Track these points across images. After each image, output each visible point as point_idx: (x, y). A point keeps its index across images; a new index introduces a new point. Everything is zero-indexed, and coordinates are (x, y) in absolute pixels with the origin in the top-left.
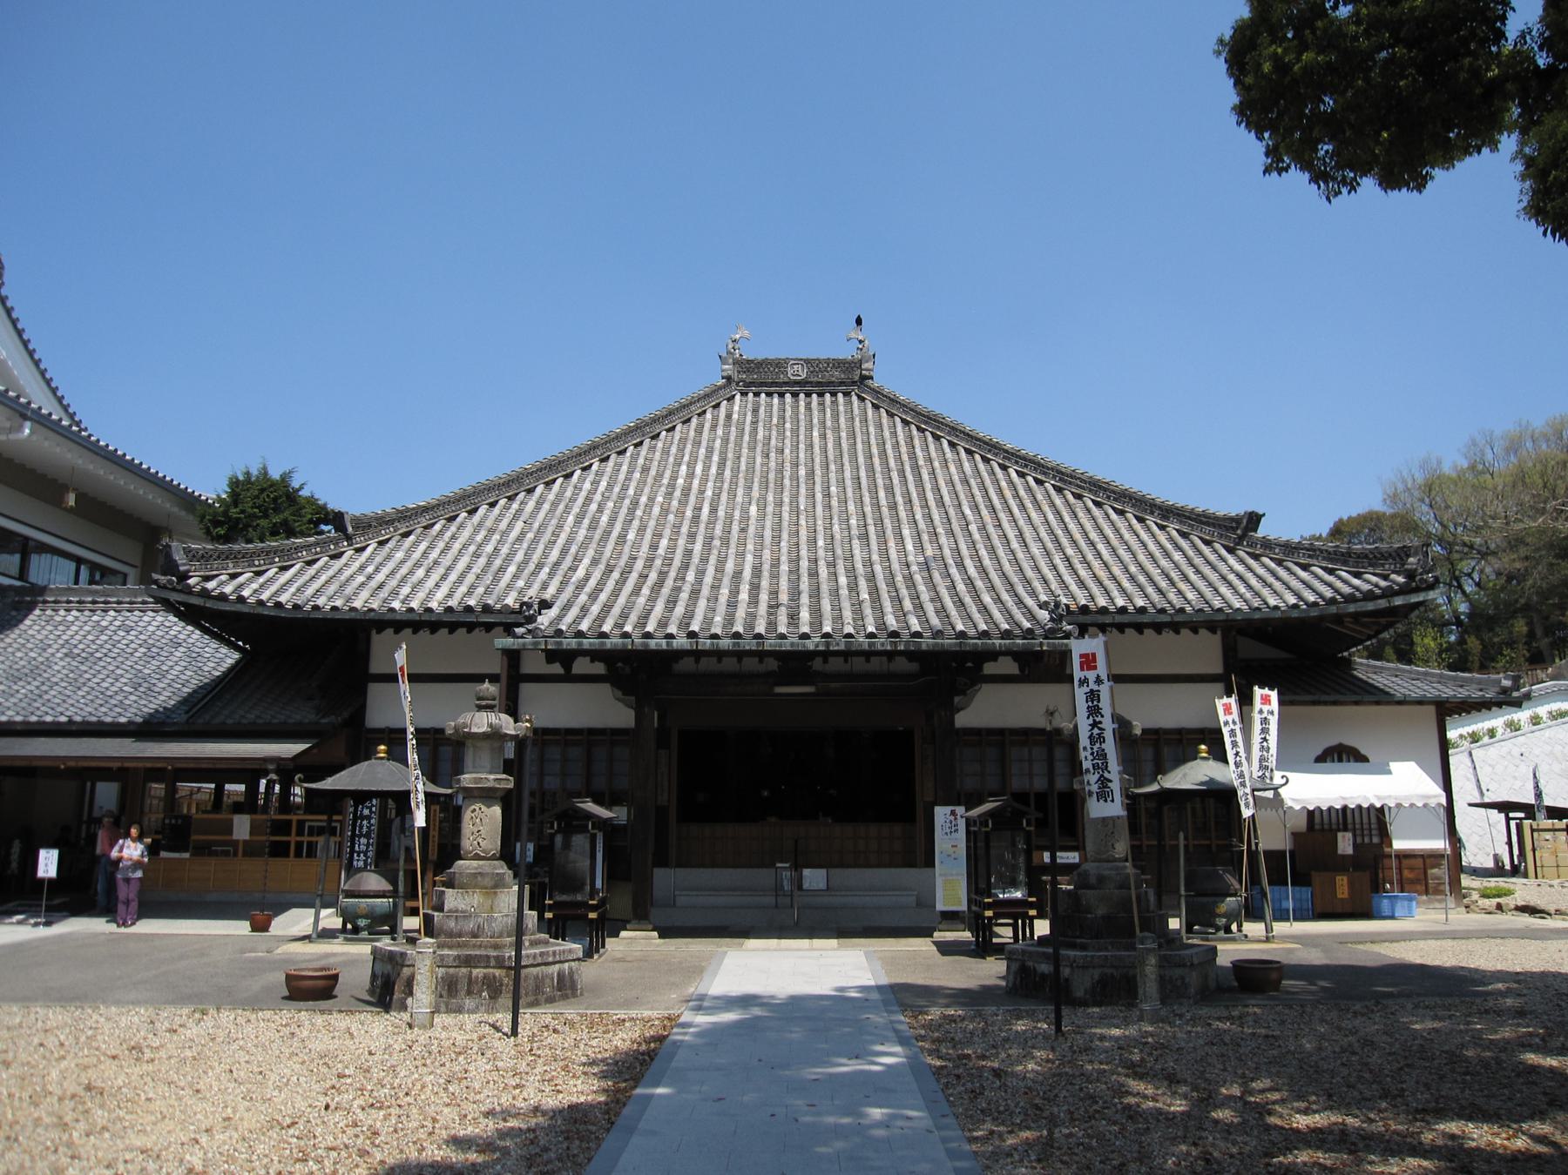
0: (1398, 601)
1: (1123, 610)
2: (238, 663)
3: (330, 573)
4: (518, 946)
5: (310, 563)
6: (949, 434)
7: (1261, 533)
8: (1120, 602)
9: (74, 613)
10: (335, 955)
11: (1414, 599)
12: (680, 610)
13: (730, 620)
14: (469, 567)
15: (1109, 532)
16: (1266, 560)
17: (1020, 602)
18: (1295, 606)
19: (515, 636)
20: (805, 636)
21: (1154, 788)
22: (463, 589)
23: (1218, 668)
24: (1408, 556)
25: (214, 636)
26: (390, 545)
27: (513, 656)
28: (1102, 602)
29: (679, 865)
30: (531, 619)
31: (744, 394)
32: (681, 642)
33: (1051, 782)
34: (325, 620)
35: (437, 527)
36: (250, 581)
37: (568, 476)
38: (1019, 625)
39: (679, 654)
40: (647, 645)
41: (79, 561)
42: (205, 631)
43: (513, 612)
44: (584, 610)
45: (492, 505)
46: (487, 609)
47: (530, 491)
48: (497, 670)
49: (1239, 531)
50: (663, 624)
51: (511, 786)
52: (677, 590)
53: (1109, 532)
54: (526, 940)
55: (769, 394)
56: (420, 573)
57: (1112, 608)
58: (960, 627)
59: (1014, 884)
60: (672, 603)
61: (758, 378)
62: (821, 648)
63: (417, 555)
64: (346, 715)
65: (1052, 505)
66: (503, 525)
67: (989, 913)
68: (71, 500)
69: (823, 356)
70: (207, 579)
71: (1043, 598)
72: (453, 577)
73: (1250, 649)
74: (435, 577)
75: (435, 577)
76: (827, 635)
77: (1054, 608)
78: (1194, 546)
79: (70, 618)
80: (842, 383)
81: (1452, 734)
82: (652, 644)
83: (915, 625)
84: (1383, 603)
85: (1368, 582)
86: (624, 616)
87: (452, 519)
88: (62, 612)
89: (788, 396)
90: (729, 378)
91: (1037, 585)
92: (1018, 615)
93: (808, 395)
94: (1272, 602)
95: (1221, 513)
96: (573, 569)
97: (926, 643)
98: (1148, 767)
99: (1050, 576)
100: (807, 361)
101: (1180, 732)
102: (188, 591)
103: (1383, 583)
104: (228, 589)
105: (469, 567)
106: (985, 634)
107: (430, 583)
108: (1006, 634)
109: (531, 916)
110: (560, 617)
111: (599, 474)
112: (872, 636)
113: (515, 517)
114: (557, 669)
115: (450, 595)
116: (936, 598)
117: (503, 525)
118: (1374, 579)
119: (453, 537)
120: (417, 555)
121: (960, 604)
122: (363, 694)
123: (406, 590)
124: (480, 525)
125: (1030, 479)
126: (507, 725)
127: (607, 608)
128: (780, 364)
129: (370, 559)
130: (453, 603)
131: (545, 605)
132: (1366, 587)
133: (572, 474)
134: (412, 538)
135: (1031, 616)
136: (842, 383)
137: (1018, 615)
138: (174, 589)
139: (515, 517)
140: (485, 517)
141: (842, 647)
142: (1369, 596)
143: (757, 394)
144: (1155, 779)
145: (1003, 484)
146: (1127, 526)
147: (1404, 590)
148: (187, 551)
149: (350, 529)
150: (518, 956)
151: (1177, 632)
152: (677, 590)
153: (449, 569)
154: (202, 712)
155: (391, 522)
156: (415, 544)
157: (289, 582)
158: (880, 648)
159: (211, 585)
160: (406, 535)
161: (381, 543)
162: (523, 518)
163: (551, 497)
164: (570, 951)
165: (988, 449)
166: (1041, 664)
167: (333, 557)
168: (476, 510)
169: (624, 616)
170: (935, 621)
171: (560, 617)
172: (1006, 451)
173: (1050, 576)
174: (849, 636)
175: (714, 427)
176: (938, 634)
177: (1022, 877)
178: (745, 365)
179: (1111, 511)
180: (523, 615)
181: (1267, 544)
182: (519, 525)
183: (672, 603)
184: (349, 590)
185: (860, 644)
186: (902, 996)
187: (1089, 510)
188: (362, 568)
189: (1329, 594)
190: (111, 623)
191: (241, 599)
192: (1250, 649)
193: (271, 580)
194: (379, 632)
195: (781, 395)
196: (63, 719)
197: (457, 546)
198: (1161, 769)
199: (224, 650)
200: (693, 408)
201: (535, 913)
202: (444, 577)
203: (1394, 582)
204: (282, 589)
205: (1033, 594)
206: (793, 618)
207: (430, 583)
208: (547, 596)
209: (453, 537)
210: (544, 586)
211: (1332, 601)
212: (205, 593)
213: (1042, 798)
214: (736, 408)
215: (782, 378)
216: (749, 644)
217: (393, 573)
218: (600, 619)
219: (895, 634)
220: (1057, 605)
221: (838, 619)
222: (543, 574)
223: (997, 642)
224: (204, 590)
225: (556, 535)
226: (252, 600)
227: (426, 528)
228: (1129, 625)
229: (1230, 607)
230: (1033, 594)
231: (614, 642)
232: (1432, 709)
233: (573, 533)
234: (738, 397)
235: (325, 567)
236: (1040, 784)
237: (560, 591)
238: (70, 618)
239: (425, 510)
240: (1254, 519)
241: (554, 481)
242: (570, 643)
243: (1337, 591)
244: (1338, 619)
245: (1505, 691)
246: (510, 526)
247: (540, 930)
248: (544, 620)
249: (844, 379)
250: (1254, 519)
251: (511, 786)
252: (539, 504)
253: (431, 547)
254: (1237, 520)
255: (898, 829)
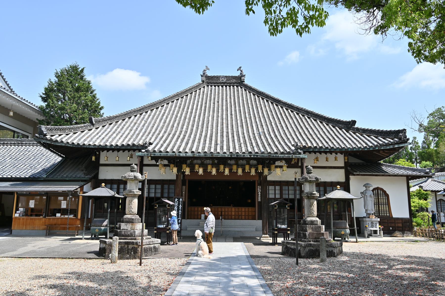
0: (396, 146)
1: (316, 147)
2: (61, 161)
3: (88, 135)
4: (142, 239)
5: (82, 132)
6: (266, 98)
7: (356, 126)
8: (315, 145)
9: (13, 146)
10: (89, 243)
11: (401, 146)
12: (189, 145)
13: (203, 148)
14: (129, 133)
15: (312, 125)
16: (357, 134)
17: (286, 144)
18: (366, 147)
19: (142, 152)
20: (225, 153)
21: (324, 198)
22: (127, 139)
23: (343, 165)
24: (399, 133)
25: (54, 153)
26: (106, 127)
27: (142, 158)
28: (310, 145)
29: (188, 219)
30: (146, 147)
31: (208, 86)
32: (190, 154)
33: (295, 196)
34: (86, 148)
35: (120, 122)
36: (65, 137)
37: (157, 108)
38: (286, 150)
39: (189, 158)
40: (179, 155)
41: (14, 132)
42: (52, 151)
43: (141, 146)
44: (162, 145)
45: (136, 116)
46: (134, 145)
47: (146, 112)
48: (137, 163)
49: (349, 126)
50: (184, 149)
51: (140, 194)
52: (188, 140)
53: (312, 125)
54: (144, 238)
55: (215, 86)
56: (115, 135)
57: (313, 147)
58: (269, 151)
59: (284, 224)
60: (187, 144)
61: (211, 81)
62: (229, 156)
63: (114, 130)
64: (93, 175)
65: (296, 118)
66: (139, 122)
67: (276, 232)
68: (11, 114)
69: (230, 75)
70: (52, 136)
71: (293, 143)
72: (124, 136)
73: (354, 160)
74: (119, 136)
75: (119, 136)
76: (231, 153)
77: (296, 147)
78: (330, 128)
79: (11, 148)
80: (236, 83)
81: (411, 184)
82: (181, 155)
83: (256, 150)
84: (391, 147)
85: (387, 140)
86: (174, 147)
87: (124, 120)
88: (9, 146)
89: (220, 86)
90: (203, 81)
91: (291, 139)
92: (286, 148)
93: (230, 86)
94: (359, 146)
95: (345, 120)
96: (159, 134)
97: (260, 155)
98: (322, 193)
99: (295, 137)
100: (226, 77)
101: (332, 183)
102: (47, 139)
103: (392, 141)
104: (58, 139)
105: (129, 133)
106: (276, 153)
107: (118, 138)
108: (282, 153)
109: (146, 231)
110: (155, 147)
111: (167, 108)
112: (244, 153)
113: (142, 120)
114: (154, 162)
115: (123, 141)
116: (262, 143)
117: (139, 122)
118: (389, 140)
119: (124, 125)
120: (114, 130)
121: (269, 145)
122: (98, 169)
123: (110, 140)
124: (132, 122)
125: (289, 110)
126: (139, 175)
127: (168, 145)
128: (218, 77)
129: (100, 131)
130: (124, 143)
131: (151, 144)
132: (387, 142)
133: (158, 108)
134: (112, 125)
135: (290, 148)
136: (236, 83)
137: (286, 148)
138: (42, 139)
139: (142, 120)
140: (134, 120)
141: (235, 156)
142: (387, 145)
143: (211, 86)
144: (325, 195)
145: (282, 112)
146: (317, 124)
147: (397, 143)
148: (46, 128)
149: (94, 122)
150: (142, 242)
151: (331, 154)
152: (188, 140)
153: (123, 134)
154: (51, 175)
155: (106, 120)
156: (113, 127)
157: (76, 137)
158: (246, 156)
159: (53, 138)
160: (110, 124)
161: (103, 126)
162: (144, 120)
163: (153, 114)
164: (157, 241)
165: (277, 102)
166: (292, 162)
167: (89, 130)
168: (131, 117)
169: (174, 147)
170: (262, 150)
171: (155, 147)
172: (283, 103)
173: (295, 137)
174: (238, 153)
175: (199, 95)
176: (263, 153)
177: (286, 223)
178: (208, 78)
179: (312, 120)
180: (144, 146)
181: (358, 130)
182: (143, 122)
183: (187, 144)
184: (94, 140)
185: (241, 155)
186: (253, 259)
187: (306, 119)
188: (98, 134)
189: (376, 144)
190: (24, 149)
191: (62, 142)
192: (354, 160)
193: (71, 137)
194: (102, 152)
195: (218, 86)
196: (9, 176)
197: (125, 127)
198: (326, 192)
199: (57, 157)
200: (193, 89)
201: (147, 230)
202: (121, 136)
203: (395, 141)
204: (74, 139)
205: (290, 142)
206: (222, 148)
207: (118, 138)
208: (151, 141)
209: (124, 125)
210: (150, 139)
211: (377, 146)
212: (51, 140)
213: (292, 201)
214: (205, 90)
215: (218, 81)
216: (209, 155)
217: (103, 139)
218: (166, 148)
219: (250, 153)
220: (297, 145)
221: (234, 148)
222: (150, 136)
223: (280, 155)
224: (51, 139)
225: (154, 125)
226: (65, 142)
227: (116, 122)
228: (317, 152)
229: (347, 147)
230: (290, 142)
231: (170, 154)
232: (405, 178)
233: (159, 124)
234: (206, 87)
235: (87, 133)
236: (291, 197)
237: (155, 140)
238: (11, 148)
239: (116, 117)
240: (354, 122)
241: (153, 109)
242: (158, 154)
243: (378, 143)
244: (378, 151)
245: (427, 173)
246: (141, 122)
247: (148, 235)
248: (150, 148)
249: (238, 81)
250: (354, 122)
251: (140, 194)
252: (149, 116)
253: (118, 128)
254: (349, 122)
255: (250, 209)
